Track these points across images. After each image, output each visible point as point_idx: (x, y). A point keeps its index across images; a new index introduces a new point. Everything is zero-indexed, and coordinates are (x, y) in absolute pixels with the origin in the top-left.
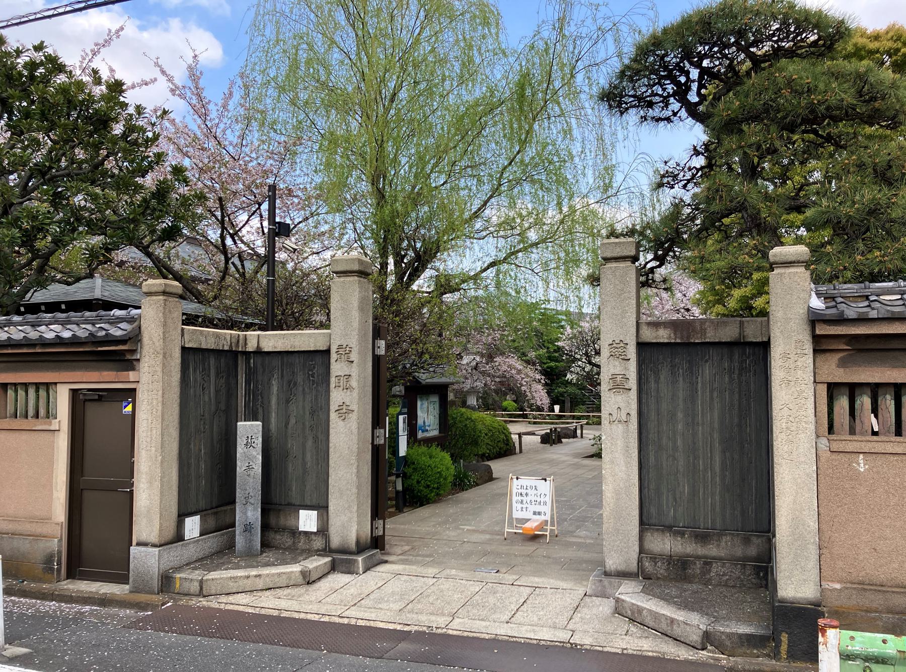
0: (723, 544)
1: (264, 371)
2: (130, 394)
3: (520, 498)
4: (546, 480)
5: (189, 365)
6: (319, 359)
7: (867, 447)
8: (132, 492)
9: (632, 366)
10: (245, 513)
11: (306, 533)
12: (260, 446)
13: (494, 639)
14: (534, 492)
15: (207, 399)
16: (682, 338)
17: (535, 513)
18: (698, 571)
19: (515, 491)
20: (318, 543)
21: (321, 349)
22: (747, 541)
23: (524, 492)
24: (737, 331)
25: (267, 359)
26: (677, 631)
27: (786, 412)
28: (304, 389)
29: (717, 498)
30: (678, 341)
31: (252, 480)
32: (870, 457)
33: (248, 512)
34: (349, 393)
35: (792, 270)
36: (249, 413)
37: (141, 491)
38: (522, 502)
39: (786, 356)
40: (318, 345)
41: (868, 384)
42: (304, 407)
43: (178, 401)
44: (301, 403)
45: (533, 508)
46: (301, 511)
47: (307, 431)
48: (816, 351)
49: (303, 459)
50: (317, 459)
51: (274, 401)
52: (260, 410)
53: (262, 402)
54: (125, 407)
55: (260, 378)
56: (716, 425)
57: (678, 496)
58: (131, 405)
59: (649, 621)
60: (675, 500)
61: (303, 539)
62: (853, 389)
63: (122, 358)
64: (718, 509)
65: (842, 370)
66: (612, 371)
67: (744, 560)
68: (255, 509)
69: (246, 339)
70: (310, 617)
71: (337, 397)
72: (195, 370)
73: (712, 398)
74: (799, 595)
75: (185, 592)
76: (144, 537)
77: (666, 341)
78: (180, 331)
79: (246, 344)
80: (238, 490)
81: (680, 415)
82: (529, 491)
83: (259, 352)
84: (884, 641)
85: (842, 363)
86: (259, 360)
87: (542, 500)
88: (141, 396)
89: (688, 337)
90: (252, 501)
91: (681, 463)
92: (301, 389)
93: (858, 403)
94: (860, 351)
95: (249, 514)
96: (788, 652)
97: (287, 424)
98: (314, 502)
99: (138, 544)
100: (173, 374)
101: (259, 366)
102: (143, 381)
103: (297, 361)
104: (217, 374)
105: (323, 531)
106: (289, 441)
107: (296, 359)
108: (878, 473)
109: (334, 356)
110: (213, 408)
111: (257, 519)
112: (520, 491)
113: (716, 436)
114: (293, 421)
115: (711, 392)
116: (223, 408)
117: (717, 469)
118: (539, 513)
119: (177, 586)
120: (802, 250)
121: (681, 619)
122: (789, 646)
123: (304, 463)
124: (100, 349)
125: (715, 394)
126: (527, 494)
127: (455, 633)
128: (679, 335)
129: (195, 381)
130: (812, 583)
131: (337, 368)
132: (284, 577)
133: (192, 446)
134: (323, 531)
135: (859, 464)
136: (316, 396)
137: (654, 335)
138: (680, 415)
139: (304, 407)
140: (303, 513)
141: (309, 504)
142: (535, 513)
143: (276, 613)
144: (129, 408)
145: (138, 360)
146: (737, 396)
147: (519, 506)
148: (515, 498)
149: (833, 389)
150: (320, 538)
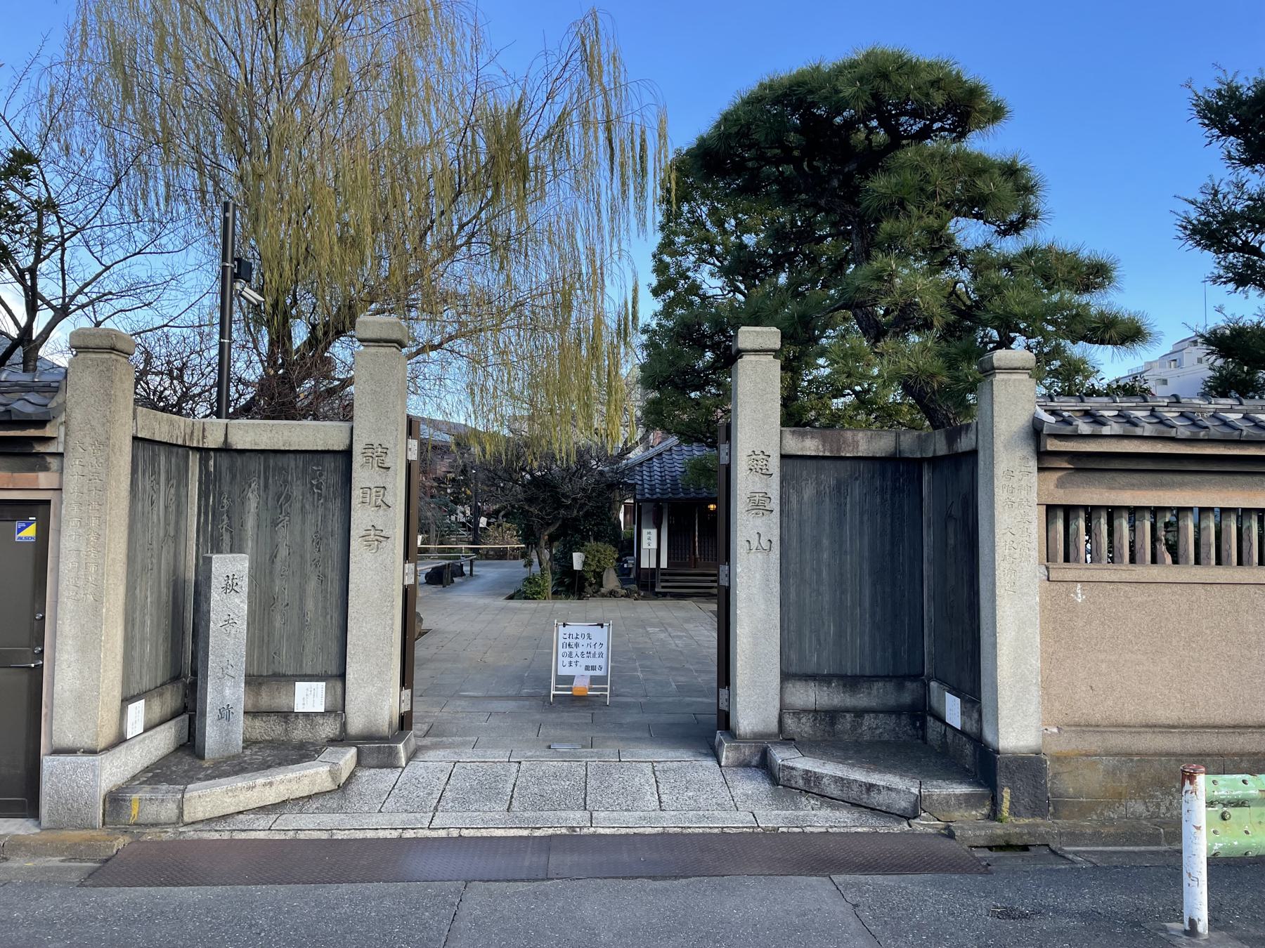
0: (874, 692)
1: (233, 477)
2: (38, 509)
3: (568, 650)
4: (602, 626)
6: (329, 463)
7: (1086, 575)
9: (775, 482)
10: (221, 692)
11: (307, 715)
12: (246, 589)
13: (662, 834)
14: (587, 641)
16: (831, 451)
17: (587, 668)
18: (849, 726)
19: (561, 641)
20: (328, 729)
21: (336, 448)
22: (900, 688)
23: (573, 642)
24: (893, 444)
25: (239, 460)
26: (878, 799)
27: (1009, 537)
28: (303, 507)
29: (867, 638)
30: (827, 454)
32: (1087, 586)
33: (225, 691)
34: (381, 512)
35: (1015, 377)
36: (206, 541)
37: (64, 666)
38: (570, 655)
39: (1010, 474)
41: (1127, 508)
42: (302, 532)
44: (298, 527)
45: (584, 662)
47: (309, 568)
48: (1040, 469)
49: (301, 608)
50: (325, 608)
51: (250, 523)
52: (226, 537)
54: (20, 530)
55: (226, 488)
56: (866, 554)
57: (822, 638)
59: (833, 790)
60: (819, 640)
61: (301, 722)
62: (1069, 511)
63: (27, 450)
64: (867, 651)
65: (1062, 491)
66: (751, 489)
67: (895, 711)
68: (236, 685)
69: (204, 430)
70: (381, 834)
71: (361, 518)
72: (144, 474)
73: (861, 522)
74: (1021, 743)
75: (151, 820)
76: (68, 740)
77: (813, 454)
79: (204, 437)
81: (826, 542)
82: (580, 641)
83: (226, 450)
84: (1244, 782)
85: (1060, 484)
86: (225, 461)
87: (598, 650)
89: (839, 450)
91: (827, 598)
92: (298, 505)
93: (1116, 523)
94: (1077, 470)
95: (227, 692)
96: (1010, 809)
98: (319, 670)
99: (57, 752)
104: (168, 480)
105: (337, 709)
106: (277, 582)
107: (291, 462)
108: (1094, 603)
109: (358, 459)
110: (162, 534)
111: (238, 699)
112: (567, 641)
113: (866, 566)
114: (283, 552)
115: (861, 515)
117: (867, 604)
118: (593, 668)
119: (134, 812)
120: (1029, 358)
121: (882, 783)
122: (1012, 803)
123: (303, 614)
125: (865, 518)
126: (577, 645)
127: (608, 831)
128: (828, 447)
129: (144, 490)
130: (1033, 730)
131: (362, 476)
132: (306, 781)
134: (337, 709)
135: (1076, 594)
136: (324, 517)
137: (800, 446)
138: (826, 542)
139: (302, 532)
140: (300, 686)
141: (309, 672)
142: (587, 668)
143: (325, 836)
144: (30, 532)
146: (889, 520)
147: (567, 660)
148: (561, 651)
149: (1051, 509)
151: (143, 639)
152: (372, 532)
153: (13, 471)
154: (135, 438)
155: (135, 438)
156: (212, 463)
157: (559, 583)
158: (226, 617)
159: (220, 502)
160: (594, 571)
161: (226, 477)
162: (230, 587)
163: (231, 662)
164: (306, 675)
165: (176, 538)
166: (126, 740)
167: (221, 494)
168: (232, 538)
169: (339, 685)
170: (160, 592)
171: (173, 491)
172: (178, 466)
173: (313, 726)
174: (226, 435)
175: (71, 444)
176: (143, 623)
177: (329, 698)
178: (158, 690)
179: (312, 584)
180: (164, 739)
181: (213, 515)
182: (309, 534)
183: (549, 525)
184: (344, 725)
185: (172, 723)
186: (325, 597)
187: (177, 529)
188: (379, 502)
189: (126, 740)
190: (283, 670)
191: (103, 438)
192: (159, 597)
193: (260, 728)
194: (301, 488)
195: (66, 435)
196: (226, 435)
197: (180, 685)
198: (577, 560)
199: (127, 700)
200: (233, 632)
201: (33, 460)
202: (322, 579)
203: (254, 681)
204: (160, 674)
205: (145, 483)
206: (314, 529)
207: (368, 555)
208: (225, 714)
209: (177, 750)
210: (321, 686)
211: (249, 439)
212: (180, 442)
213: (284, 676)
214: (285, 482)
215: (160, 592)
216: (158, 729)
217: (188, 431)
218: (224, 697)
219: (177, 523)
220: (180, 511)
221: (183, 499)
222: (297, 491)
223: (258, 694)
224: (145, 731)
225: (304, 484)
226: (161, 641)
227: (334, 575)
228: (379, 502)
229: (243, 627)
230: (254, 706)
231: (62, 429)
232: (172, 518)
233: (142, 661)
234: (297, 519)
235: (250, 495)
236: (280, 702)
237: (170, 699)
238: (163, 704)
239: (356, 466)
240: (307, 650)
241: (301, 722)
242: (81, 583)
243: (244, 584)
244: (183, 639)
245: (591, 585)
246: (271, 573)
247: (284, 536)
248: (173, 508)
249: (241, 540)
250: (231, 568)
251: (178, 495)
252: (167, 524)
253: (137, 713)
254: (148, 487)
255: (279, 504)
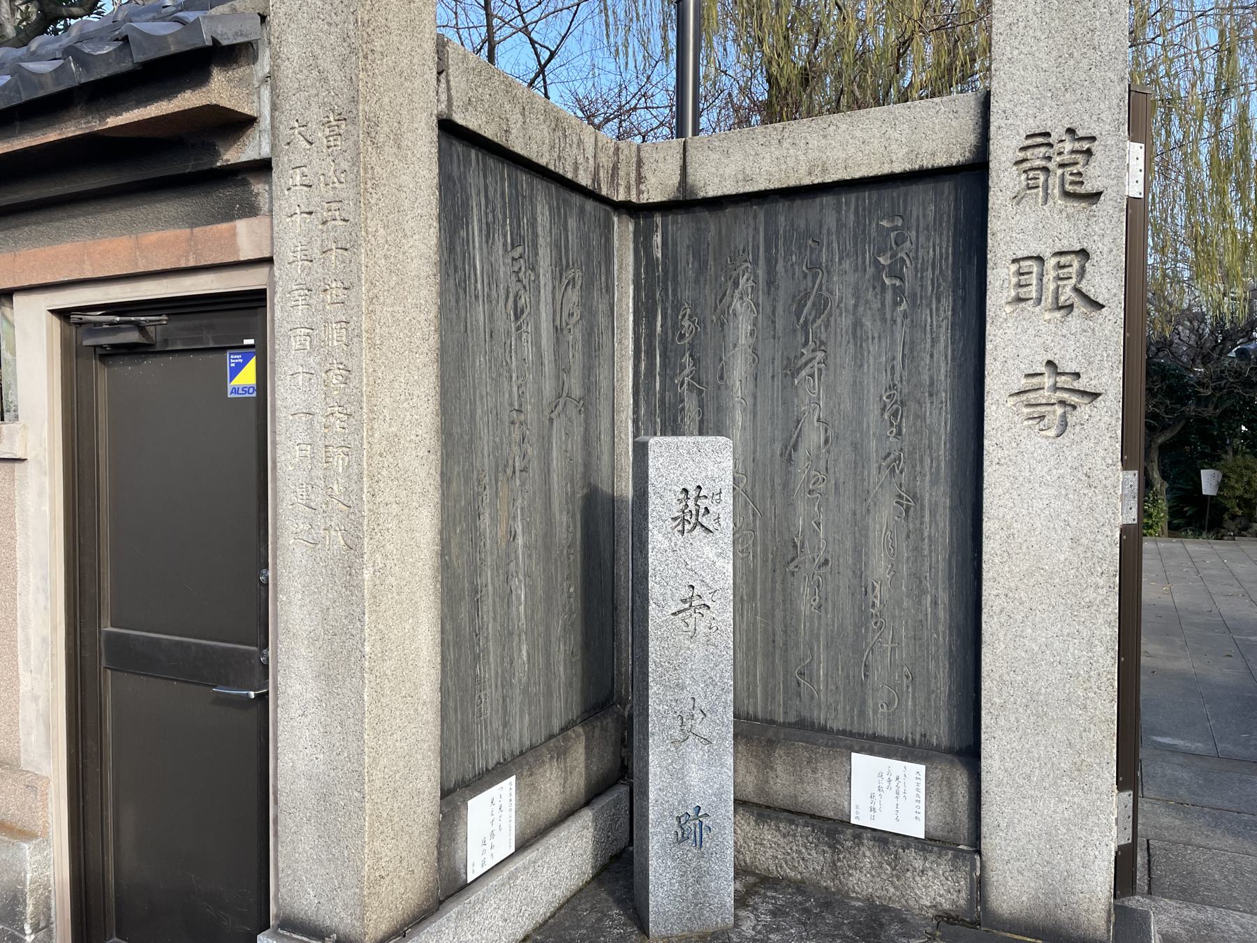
1: (702, 268)
5: (466, 206)
6: (926, 206)
8: (263, 698)
10: (679, 775)
11: (883, 839)
12: (727, 523)
15: (528, 351)
21: (941, 161)
25: (712, 224)
28: (858, 324)
31: (700, 653)
34: (1074, 321)
36: (650, 413)
37: (295, 711)
40: (927, 146)
42: (857, 388)
43: (434, 340)
46: (855, 756)
47: (874, 475)
49: (859, 574)
50: (917, 577)
51: (739, 370)
52: (691, 404)
53: (696, 378)
55: (687, 294)
58: (252, 365)
61: (868, 855)
69: (640, 163)
71: (1018, 340)
78: (430, 47)
79: (640, 179)
80: (654, 689)
83: (686, 204)
86: (682, 226)
88: (285, 314)
90: (702, 729)
92: (845, 322)
95: (695, 776)
97: (790, 448)
98: (906, 728)
100: (410, 225)
101: (682, 250)
102: (288, 251)
103: (831, 221)
104: (560, 267)
106: (801, 507)
107: (826, 211)
109: (1004, 179)
110: (548, 388)
111: (719, 795)
114: (813, 437)
116: (577, 392)
124: (113, 121)
131: (1019, 225)
133: (486, 520)
134: (961, 838)
136: (911, 348)
139: (857, 388)
141: (883, 729)
144: (247, 376)
145: (263, 167)
150: (943, 867)
151: (507, 636)
152: (1047, 381)
153: (193, 225)
154: (448, 128)
155: (448, 128)
156: (658, 239)
157: (1174, 512)
158: (685, 593)
159: (676, 326)
160: (1240, 497)
161: (688, 267)
162: (691, 518)
163: (702, 703)
164: (874, 737)
165: (587, 404)
166: (465, 887)
167: (677, 307)
168: (701, 405)
169: (961, 780)
170: (549, 521)
171: (574, 296)
172: (585, 240)
173: (900, 871)
174: (684, 168)
175: (284, 131)
176: (506, 598)
177: (937, 806)
178: (551, 744)
179: (884, 516)
180: (571, 855)
181: (664, 356)
182: (874, 391)
183: (1165, 428)
184: (979, 886)
185: (587, 816)
186: (917, 549)
187: (590, 387)
188: (1067, 295)
189: (465, 887)
190: (821, 716)
191: (342, 102)
192: (548, 534)
193: (777, 849)
194: (851, 278)
195: (274, 107)
196: (684, 168)
197: (609, 722)
198: (1209, 482)
199: (455, 792)
200: (702, 629)
201: (226, 193)
202: (909, 503)
203: (755, 732)
204: (558, 705)
205: (489, 257)
206: (884, 379)
207: (1039, 443)
208: (691, 829)
209: (593, 878)
210: (915, 772)
211: (730, 170)
212: (584, 180)
213: (824, 729)
214: (814, 267)
215: (549, 521)
216: (552, 840)
217: (605, 161)
218: (687, 788)
219: (589, 369)
220: (596, 348)
221: (602, 320)
222: (841, 285)
223: (766, 766)
224: (523, 845)
225: (860, 268)
226: (557, 630)
227: (938, 497)
228: (1067, 295)
229: (723, 614)
230: (761, 790)
231: (266, 93)
232: (576, 359)
233: (506, 684)
234: (843, 353)
235: (737, 304)
236: (816, 791)
237: (559, 781)
238: (567, 773)
239: (999, 198)
240: (876, 676)
241: (868, 855)
242: (317, 500)
243: (723, 510)
244: (614, 623)
245: (1234, 517)
246: (785, 485)
247: (814, 399)
248: (576, 335)
249: (719, 409)
250: (693, 471)
251: (589, 312)
252: (562, 369)
253: (492, 818)
254: (503, 271)
255: (755, 714)
